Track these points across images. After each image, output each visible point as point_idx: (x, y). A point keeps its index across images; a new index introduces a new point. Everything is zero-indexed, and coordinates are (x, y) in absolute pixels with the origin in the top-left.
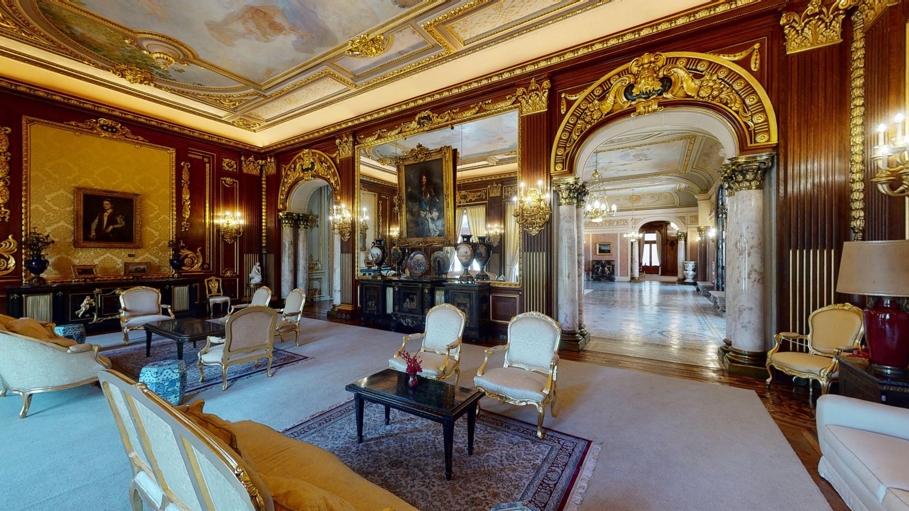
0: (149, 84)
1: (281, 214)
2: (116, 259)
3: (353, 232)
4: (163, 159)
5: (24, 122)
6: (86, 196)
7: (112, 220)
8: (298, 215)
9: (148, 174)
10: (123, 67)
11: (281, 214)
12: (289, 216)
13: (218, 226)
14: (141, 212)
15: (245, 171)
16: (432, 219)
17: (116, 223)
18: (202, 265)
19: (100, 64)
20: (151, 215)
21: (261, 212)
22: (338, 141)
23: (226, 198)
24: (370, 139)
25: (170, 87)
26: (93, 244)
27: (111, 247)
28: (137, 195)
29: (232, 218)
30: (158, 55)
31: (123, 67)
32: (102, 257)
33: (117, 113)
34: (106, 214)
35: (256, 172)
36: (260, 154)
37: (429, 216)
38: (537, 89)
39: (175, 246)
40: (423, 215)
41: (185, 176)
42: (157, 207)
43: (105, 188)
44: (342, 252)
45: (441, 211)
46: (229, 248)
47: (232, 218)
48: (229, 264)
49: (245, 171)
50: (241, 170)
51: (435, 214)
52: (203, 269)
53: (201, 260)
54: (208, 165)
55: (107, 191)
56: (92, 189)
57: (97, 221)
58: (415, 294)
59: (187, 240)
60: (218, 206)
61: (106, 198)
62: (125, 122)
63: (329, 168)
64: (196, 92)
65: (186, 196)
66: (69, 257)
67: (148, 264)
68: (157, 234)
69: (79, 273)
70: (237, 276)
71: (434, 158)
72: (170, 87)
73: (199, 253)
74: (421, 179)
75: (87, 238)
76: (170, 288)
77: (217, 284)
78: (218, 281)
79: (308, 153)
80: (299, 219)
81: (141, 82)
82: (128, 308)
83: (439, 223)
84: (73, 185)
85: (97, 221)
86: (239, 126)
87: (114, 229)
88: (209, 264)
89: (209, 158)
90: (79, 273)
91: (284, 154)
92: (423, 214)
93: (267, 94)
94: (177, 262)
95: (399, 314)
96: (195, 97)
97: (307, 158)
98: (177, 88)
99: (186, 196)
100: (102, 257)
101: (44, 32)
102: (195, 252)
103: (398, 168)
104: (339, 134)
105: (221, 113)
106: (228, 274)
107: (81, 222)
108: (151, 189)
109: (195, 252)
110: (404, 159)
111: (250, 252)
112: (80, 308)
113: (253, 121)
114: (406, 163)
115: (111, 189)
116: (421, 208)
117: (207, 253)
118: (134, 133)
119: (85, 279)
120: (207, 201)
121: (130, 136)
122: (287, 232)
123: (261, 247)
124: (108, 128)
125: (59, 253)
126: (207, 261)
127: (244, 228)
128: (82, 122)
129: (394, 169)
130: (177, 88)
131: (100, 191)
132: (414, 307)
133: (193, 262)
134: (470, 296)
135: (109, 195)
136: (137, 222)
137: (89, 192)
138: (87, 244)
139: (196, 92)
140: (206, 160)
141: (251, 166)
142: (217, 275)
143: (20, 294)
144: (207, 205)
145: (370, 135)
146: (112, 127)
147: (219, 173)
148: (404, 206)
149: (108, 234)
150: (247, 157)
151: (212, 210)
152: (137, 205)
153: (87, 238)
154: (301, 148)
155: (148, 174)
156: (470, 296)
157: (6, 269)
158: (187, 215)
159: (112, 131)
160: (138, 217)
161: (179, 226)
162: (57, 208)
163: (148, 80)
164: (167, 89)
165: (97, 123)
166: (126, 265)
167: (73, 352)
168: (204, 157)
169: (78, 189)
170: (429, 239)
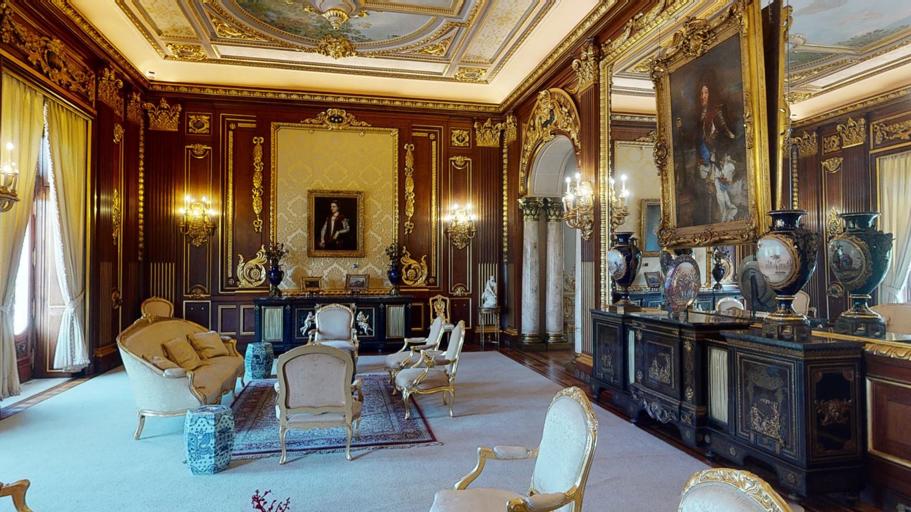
0: (351, 55)
1: (520, 201)
2: (341, 269)
3: (596, 224)
4: (384, 143)
5: (272, 129)
6: (317, 200)
7: (338, 226)
8: (545, 200)
9: (364, 163)
10: (323, 42)
11: (520, 201)
12: (531, 203)
13: (446, 224)
14: (364, 213)
15: (480, 144)
16: (722, 180)
17: (342, 228)
18: (427, 279)
19: (307, 47)
20: (374, 216)
21: (502, 201)
22: (838, 127)
23: (454, 184)
24: (619, 41)
25: (370, 51)
26: (323, 253)
27: (337, 256)
28: (359, 193)
29: (461, 213)
30: (332, 12)
31: (323, 42)
32: (330, 269)
33: (341, 100)
34: (333, 218)
35: (494, 143)
36: (497, 115)
37: (717, 173)
38: (168, 109)
39: (396, 256)
40: (704, 175)
41: (409, 162)
42: (379, 206)
43: (333, 189)
44: (583, 261)
45: (740, 158)
46: (460, 255)
47: (461, 213)
48: (460, 279)
49: (480, 144)
50: (475, 142)
51: (728, 168)
52: (429, 284)
53: (426, 272)
54: (434, 143)
55: (333, 192)
56: (322, 192)
57: (325, 226)
58: (667, 351)
59: (410, 243)
60: (446, 197)
61: (331, 200)
62: (350, 108)
63: (569, 113)
64: (394, 47)
65: (410, 188)
66: (305, 268)
67: (367, 277)
68: (380, 239)
69: (307, 286)
70: (469, 296)
71: (722, 38)
72: (370, 51)
73: (424, 263)
74: (699, 93)
75: (318, 247)
76: (384, 309)
77: (443, 306)
78: (445, 301)
79: (546, 95)
80: (546, 208)
81: (344, 55)
82: (321, 330)
83: (737, 187)
84: (308, 188)
85: (325, 226)
86: (462, 80)
87: (340, 234)
88: (435, 278)
89: (435, 133)
90: (307, 286)
91: (521, 107)
92: (704, 171)
93: (464, 20)
94: (396, 275)
95: (643, 389)
96: (396, 55)
97: (544, 107)
98: (376, 50)
99: (410, 188)
100: (330, 269)
101: (255, 29)
102: (419, 261)
103: (657, 82)
104: (574, 53)
105: (438, 68)
106: (459, 292)
107: (313, 227)
108: (375, 183)
109: (419, 261)
110: (666, 61)
111: (486, 261)
112: (303, 325)
113: (476, 67)
114: (672, 68)
115: (338, 189)
116: (701, 160)
117: (433, 263)
118: (358, 119)
119: (312, 292)
120: (434, 192)
121: (355, 123)
122: (529, 226)
123: (501, 253)
124: (335, 118)
125: (297, 263)
126: (433, 274)
127: (477, 225)
128: (315, 117)
129: (649, 85)
130: (376, 50)
131: (328, 192)
132: (666, 380)
133: (416, 276)
134: (783, 374)
135: (336, 195)
136: (360, 225)
137: (319, 195)
138: (318, 253)
139: (394, 47)
140: (432, 137)
141: (488, 134)
142: (445, 293)
143: (384, 305)
144: (434, 197)
145: (620, 32)
146: (339, 117)
147: (449, 151)
148: (670, 161)
149: (335, 241)
150: (482, 120)
151: (439, 204)
152: (360, 207)
153: (318, 247)
154: (536, 93)
155: (364, 163)
156: (783, 374)
157: (260, 280)
158: (410, 212)
159: (339, 122)
160: (361, 218)
161: (401, 227)
162: (295, 215)
163: (348, 50)
164: (371, 55)
165: (326, 115)
166: (348, 277)
167: (168, 377)
168: (429, 133)
169: (310, 192)
170: (717, 228)
